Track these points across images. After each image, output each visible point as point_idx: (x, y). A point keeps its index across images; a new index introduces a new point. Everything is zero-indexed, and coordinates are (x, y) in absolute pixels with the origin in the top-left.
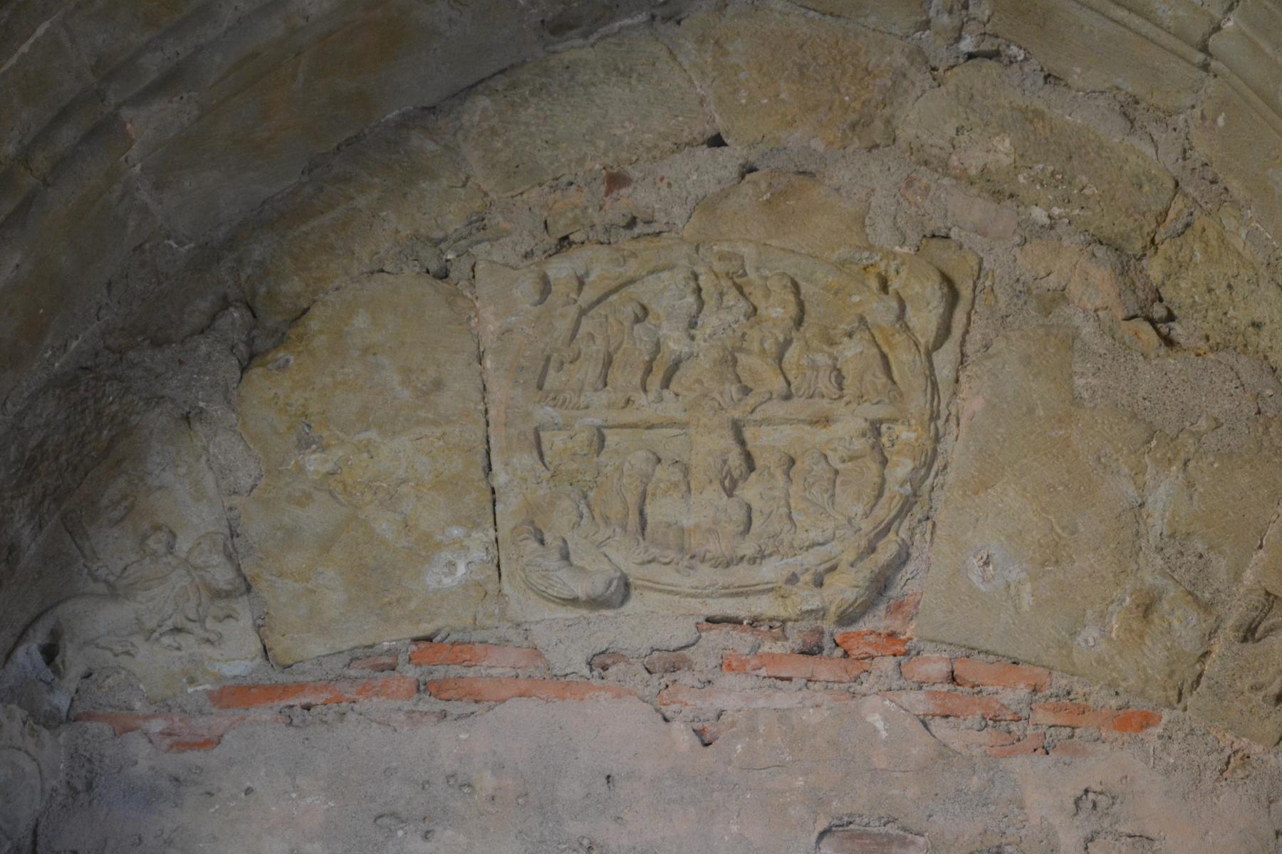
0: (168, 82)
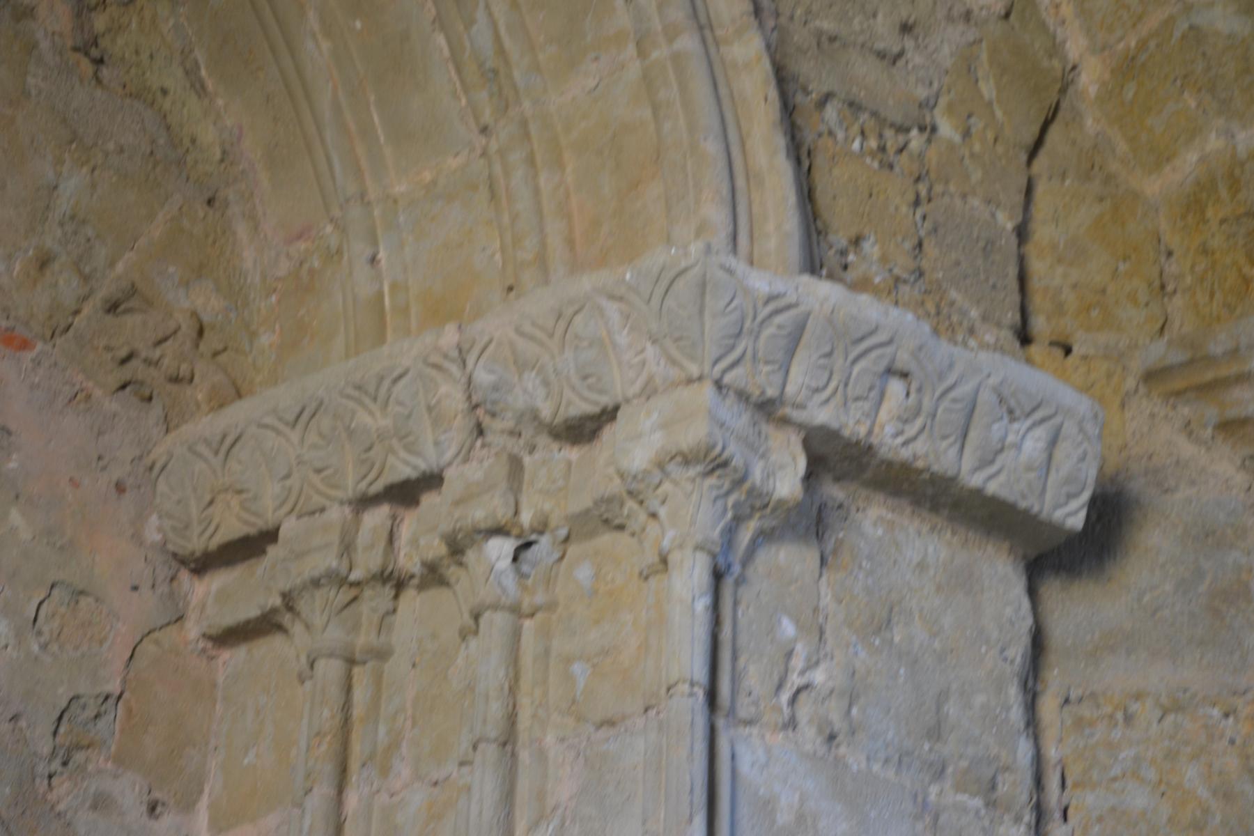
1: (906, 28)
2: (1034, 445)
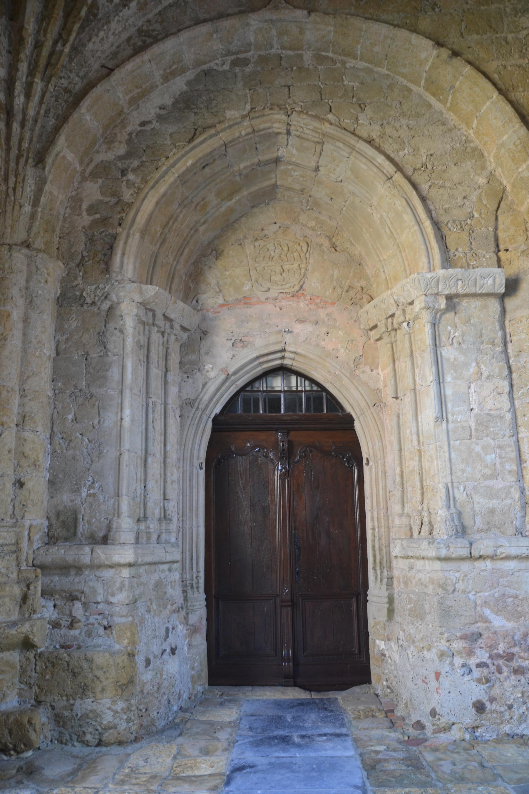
1: (465, 198)
2: (490, 281)
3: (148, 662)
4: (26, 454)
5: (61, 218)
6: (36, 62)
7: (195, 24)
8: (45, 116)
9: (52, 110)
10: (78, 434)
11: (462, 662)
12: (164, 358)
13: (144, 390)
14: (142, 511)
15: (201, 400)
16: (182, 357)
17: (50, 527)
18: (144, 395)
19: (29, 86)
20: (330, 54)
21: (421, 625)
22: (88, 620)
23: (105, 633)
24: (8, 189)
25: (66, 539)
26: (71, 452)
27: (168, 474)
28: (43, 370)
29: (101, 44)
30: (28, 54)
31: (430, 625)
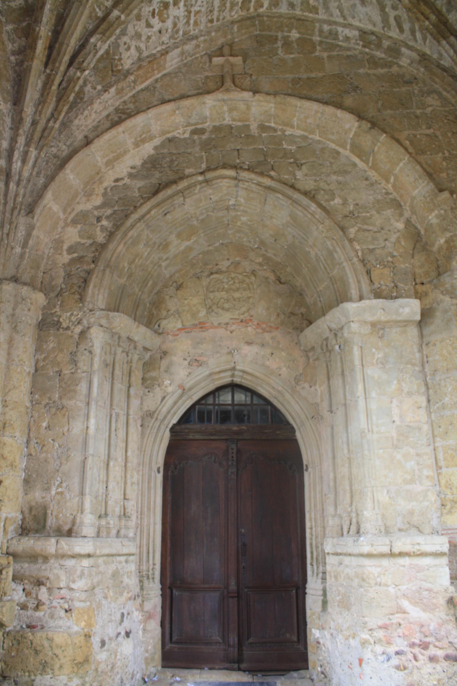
0: (167, 259)
1: (386, 240)
3: (103, 643)
4: (5, 456)
5: (46, 256)
6: (32, 136)
7: (162, 104)
8: (36, 176)
9: (43, 172)
10: (50, 440)
11: (382, 650)
12: (128, 375)
13: (108, 402)
14: (104, 509)
15: (160, 411)
16: (144, 374)
17: (23, 520)
18: (109, 406)
19: (26, 154)
20: (273, 125)
21: (347, 615)
22: (51, 603)
23: (66, 616)
24: (3, 234)
25: (37, 531)
26: (44, 455)
27: (128, 476)
28: (22, 384)
29: (85, 121)
30: (25, 129)
31: (355, 615)
